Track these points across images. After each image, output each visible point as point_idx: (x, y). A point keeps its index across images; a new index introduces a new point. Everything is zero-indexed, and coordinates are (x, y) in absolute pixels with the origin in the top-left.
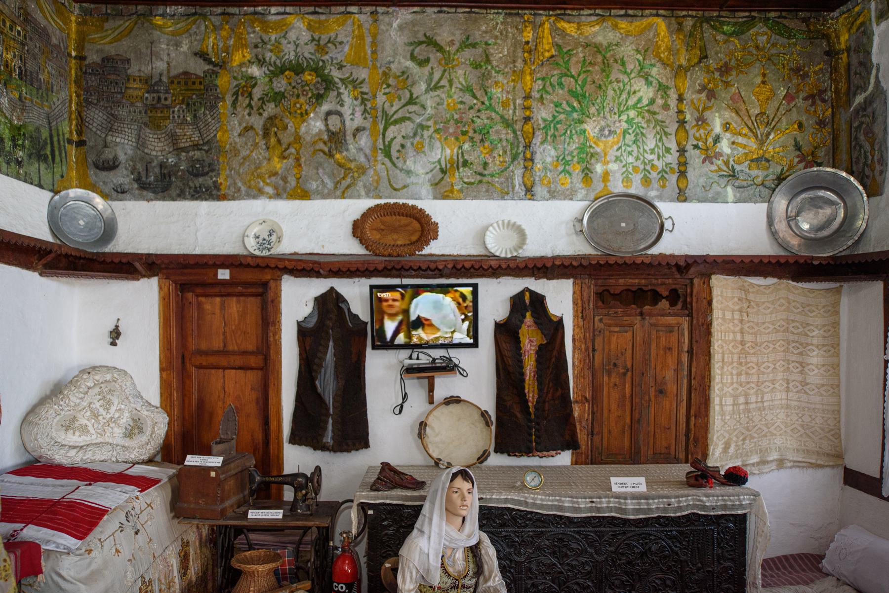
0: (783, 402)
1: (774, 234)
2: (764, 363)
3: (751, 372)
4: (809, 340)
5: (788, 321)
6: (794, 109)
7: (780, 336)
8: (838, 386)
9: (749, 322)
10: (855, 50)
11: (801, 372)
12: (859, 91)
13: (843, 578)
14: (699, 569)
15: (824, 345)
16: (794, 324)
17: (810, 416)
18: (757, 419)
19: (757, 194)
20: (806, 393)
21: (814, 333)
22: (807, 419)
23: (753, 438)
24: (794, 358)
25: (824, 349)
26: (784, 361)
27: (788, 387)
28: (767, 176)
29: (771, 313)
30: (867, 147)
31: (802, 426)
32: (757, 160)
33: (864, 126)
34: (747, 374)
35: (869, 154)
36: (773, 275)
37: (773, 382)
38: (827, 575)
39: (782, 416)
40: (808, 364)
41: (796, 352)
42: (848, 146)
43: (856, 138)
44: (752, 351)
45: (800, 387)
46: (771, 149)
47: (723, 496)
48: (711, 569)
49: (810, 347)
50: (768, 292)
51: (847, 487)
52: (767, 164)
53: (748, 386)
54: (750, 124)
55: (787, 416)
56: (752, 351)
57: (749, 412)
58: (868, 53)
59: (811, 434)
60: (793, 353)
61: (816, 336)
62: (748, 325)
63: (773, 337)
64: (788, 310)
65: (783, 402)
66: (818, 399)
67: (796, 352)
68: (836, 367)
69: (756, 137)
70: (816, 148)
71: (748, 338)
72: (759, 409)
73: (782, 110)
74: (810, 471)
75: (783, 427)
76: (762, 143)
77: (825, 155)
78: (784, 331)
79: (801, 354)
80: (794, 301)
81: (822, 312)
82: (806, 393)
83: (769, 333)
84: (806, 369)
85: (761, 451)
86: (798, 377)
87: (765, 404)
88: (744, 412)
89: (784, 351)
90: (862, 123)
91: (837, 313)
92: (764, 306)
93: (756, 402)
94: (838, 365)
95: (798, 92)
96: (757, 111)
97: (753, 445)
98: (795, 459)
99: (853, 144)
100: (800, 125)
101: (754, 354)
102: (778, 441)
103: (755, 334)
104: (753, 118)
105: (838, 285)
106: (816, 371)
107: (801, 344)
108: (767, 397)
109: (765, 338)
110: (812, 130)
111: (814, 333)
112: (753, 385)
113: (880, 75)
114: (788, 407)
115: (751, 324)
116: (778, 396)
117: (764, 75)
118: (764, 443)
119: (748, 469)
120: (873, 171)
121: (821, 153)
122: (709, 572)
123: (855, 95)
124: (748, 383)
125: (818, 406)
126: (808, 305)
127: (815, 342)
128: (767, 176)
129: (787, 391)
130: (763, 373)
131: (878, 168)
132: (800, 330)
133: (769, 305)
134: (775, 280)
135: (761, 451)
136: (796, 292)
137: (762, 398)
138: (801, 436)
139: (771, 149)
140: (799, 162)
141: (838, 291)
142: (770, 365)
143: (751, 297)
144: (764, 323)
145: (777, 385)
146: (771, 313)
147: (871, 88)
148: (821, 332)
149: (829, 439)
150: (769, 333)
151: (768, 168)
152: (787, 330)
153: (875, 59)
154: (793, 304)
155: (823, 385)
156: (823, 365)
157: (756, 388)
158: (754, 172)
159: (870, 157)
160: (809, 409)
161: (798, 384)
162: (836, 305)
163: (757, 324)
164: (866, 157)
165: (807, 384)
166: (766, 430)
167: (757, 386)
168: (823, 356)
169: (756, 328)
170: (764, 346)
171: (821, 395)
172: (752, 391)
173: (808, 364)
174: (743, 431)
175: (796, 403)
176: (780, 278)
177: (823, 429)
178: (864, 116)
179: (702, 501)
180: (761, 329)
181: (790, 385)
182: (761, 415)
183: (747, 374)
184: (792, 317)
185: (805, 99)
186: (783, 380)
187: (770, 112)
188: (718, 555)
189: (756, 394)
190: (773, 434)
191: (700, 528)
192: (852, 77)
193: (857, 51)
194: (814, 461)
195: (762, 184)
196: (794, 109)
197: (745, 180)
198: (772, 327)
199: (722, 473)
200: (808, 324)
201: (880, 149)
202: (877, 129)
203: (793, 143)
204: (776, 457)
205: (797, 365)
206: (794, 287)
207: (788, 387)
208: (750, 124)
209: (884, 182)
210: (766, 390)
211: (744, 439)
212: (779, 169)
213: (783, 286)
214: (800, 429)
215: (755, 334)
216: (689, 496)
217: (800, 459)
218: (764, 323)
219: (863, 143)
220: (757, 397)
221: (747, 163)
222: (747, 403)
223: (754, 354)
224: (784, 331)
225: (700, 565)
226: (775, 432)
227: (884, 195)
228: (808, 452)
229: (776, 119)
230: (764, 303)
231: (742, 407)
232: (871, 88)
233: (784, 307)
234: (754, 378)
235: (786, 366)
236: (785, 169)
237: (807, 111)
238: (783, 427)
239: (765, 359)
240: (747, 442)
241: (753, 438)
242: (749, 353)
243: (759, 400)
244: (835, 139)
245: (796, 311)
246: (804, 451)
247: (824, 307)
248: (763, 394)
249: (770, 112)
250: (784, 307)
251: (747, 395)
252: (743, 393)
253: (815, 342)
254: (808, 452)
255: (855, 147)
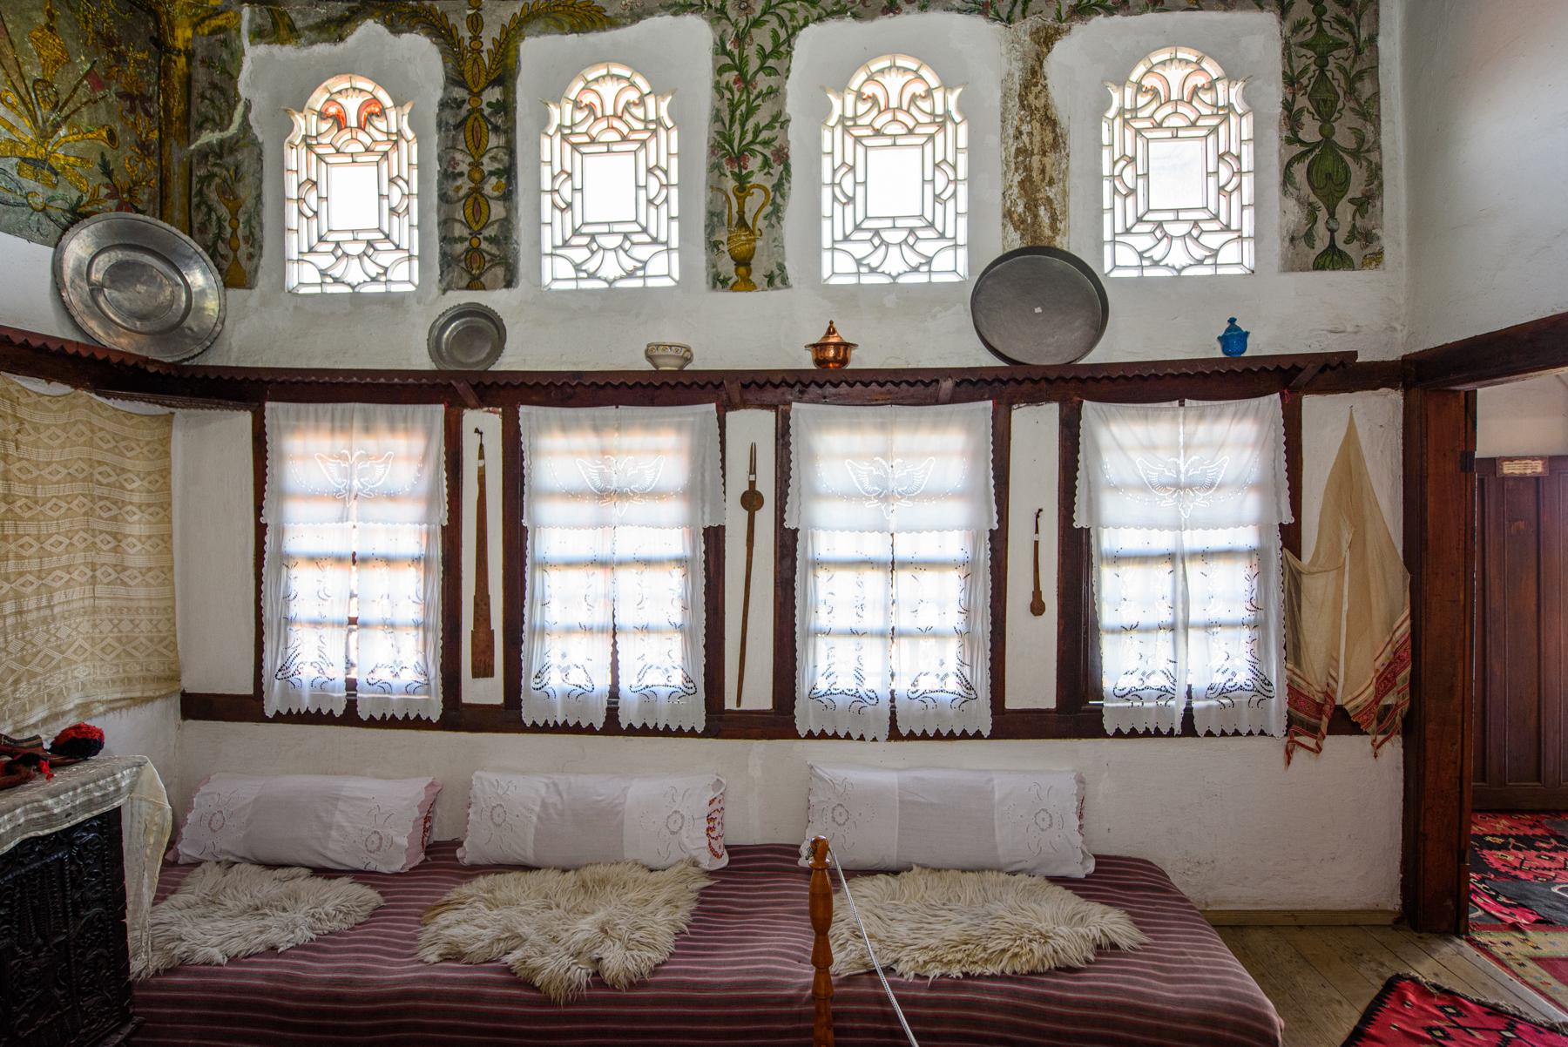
0: (87, 603)
1: (65, 307)
2: (50, 536)
3: (25, 553)
4: (127, 497)
5: (91, 462)
6: (102, 104)
7: (78, 487)
8: (171, 568)
9: (20, 459)
10: (203, 61)
11: (115, 550)
12: (209, 125)
13: (222, 858)
14: (39, 949)
15: (149, 505)
16: (101, 469)
17: (132, 621)
18: (39, 640)
19: (34, 226)
20: (124, 583)
21: (134, 486)
22: (126, 627)
23: (35, 675)
24: (102, 526)
25: (151, 510)
26: (85, 531)
27: (93, 577)
28: (52, 199)
29: (62, 446)
30: (224, 211)
31: (119, 640)
32: (34, 163)
33: (217, 180)
34: (19, 557)
35: (226, 224)
36: (64, 380)
37: (68, 569)
38: (198, 864)
39: (85, 627)
40: (126, 536)
41: (105, 515)
42: (185, 200)
43: (200, 192)
44: (27, 515)
45: (114, 575)
46: (60, 153)
47: (84, 784)
48: (62, 938)
49: (129, 508)
50: (55, 407)
51: (189, 722)
52: (54, 179)
53: (22, 580)
54: (23, 92)
55: (95, 626)
56: (27, 515)
57: (26, 628)
58: (232, 78)
59: (165, 651)
60: (100, 517)
61: (136, 489)
62: (18, 465)
63: (66, 489)
64: (90, 443)
65: (87, 603)
66: (141, 592)
67: (105, 515)
68: (167, 538)
69: (35, 121)
70: (135, 183)
71: (18, 489)
72: (45, 621)
73: (82, 94)
74: (134, 711)
75: (87, 646)
76: (44, 136)
77: (149, 201)
78: (84, 480)
79: (114, 518)
80: (101, 429)
81: (145, 450)
82: (124, 583)
83: (58, 482)
84: (123, 545)
85: (50, 696)
86: (110, 558)
87: (56, 610)
88: (14, 630)
89: (86, 514)
90: (214, 175)
91: (167, 454)
92: (50, 432)
93: (39, 609)
94: (171, 537)
95: (108, 77)
96: (37, 74)
97: (34, 688)
98: (110, 697)
99: (195, 200)
100: (112, 137)
101: (31, 519)
102: (81, 672)
103: (34, 482)
104: (30, 85)
105: (167, 410)
106: (139, 546)
107: (115, 503)
108: (58, 597)
109: (51, 491)
110: (130, 153)
111: (134, 486)
112: (30, 578)
113: (251, 117)
114: (95, 610)
115: (24, 463)
116: (76, 593)
117: (51, 16)
118: (56, 681)
119: (95, 723)
120: (235, 251)
121: (143, 196)
122: (58, 945)
123: (200, 127)
124: (21, 574)
125: (143, 604)
126: (124, 439)
127: (136, 498)
128: (52, 199)
129: (94, 584)
130: (50, 555)
131: (244, 249)
132: (112, 479)
133: (59, 432)
134: (67, 389)
135: (50, 696)
136: (105, 414)
137: (50, 599)
138: (118, 656)
139: (60, 153)
140: (109, 196)
141: (168, 420)
142: (61, 538)
143: (23, 413)
144: (49, 464)
145: (75, 575)
146: (62, 446)
147: (233, 129)
148: (145, 483)
149: (161, 654)
150: (58, 482)
151: (55, 186)
152: (89, 479)
153: (243, 89)
154: (101, 434)
155: (150, 569)
156: (149, 537)
157: (37, 583)
158: (29, 184)
159: (229, 230)
160: (129, 609)
161: (110, 570)
162: (166, 441)
163: (37, 466)
164: (221, 227)
165: (125, 569)
166: (58, 656)
167: (39, 578)
168: (149, 522)
169: (36, 473)
170: (49, 505)
171: (148, 585)
172: (29, 590)
173: (126, 536)
174: (14, 666)
175: (109, 603)
176: (76, 387)
177: (151, 640)
178: (215, 165)
179: (44, 809)
180: (45, 473)
181: (98, 573)
182: (47, 631)
183: (19, 557)
184: (97, 457)
185: (120, 95)
186: (86, 564)
187: (62, 86)
188: (74, 904)
189: (38, 593)
190: (70, 662)
191: (36, 865)
192: (195, 99)
193: (208, 63)
194: (138, 694)
195: (44, 210)
196: (102, 104)
197: (10, 191)
198: (64, 472)
199: (47, 746)
200: (123, 470)
201: (248, 222)
202: (245, 192)
203: (99, 160)
204: (77, 701)
205: (109, 538)
206: (100, 405)
207: (93, 577)
208: (23, 92)
209: (256, 271)
210: (58, 584)
211: (17, 682)
212: (74, 195)
213: (81, 401)
214: (116, 645)
215: (34, 482)
216: (16, 807)
217: (118, 696)
218: (49, 464)
219: (216, 205)
220: (39, 600)
221: (15, 160)
222: (20, 613)
223: (31, 519)
224: (84, 480)
225: (39, 941)
226: (74, 657)
227: (256, 292)
228: (128, 681)
229: (71, 106)
230: (48, 427)
231: (10, 621)
232: (233, 129)
233: (82, 439)
234: (34, 565)
235: (90, 539)
236: (85, 199)
237: (124, 118)
238: (87, 646)
239: (53, 529)
240: (23, 685)
241: (35, 675)
242: (21, 519)
243: (44, 603)
244: (164, 181)
245: (105, 447)
246: (122, 681)
247: (148, 443)
248: (51, 592)
249: (62, 86)
250: (82, 439)
251: (19, 597)
252: (11, 594)
253: (136, 498)
254: (128, 681)
255: (198, 206)
